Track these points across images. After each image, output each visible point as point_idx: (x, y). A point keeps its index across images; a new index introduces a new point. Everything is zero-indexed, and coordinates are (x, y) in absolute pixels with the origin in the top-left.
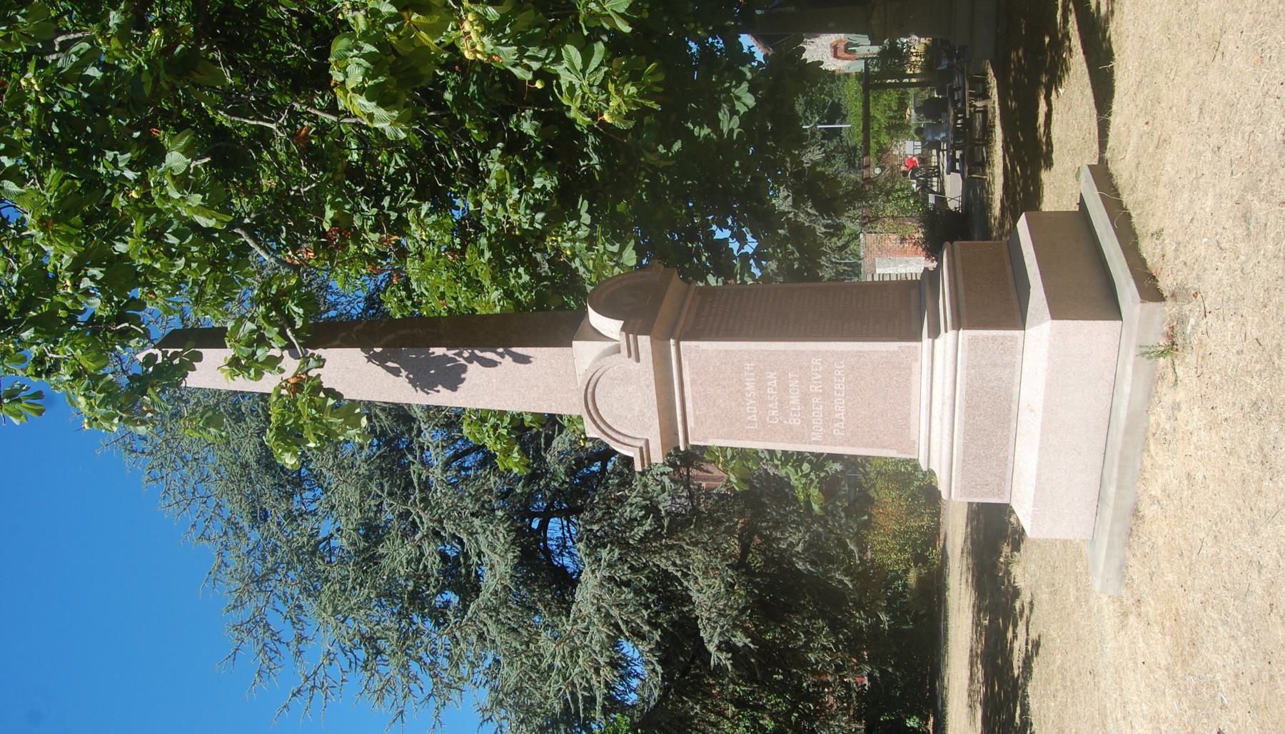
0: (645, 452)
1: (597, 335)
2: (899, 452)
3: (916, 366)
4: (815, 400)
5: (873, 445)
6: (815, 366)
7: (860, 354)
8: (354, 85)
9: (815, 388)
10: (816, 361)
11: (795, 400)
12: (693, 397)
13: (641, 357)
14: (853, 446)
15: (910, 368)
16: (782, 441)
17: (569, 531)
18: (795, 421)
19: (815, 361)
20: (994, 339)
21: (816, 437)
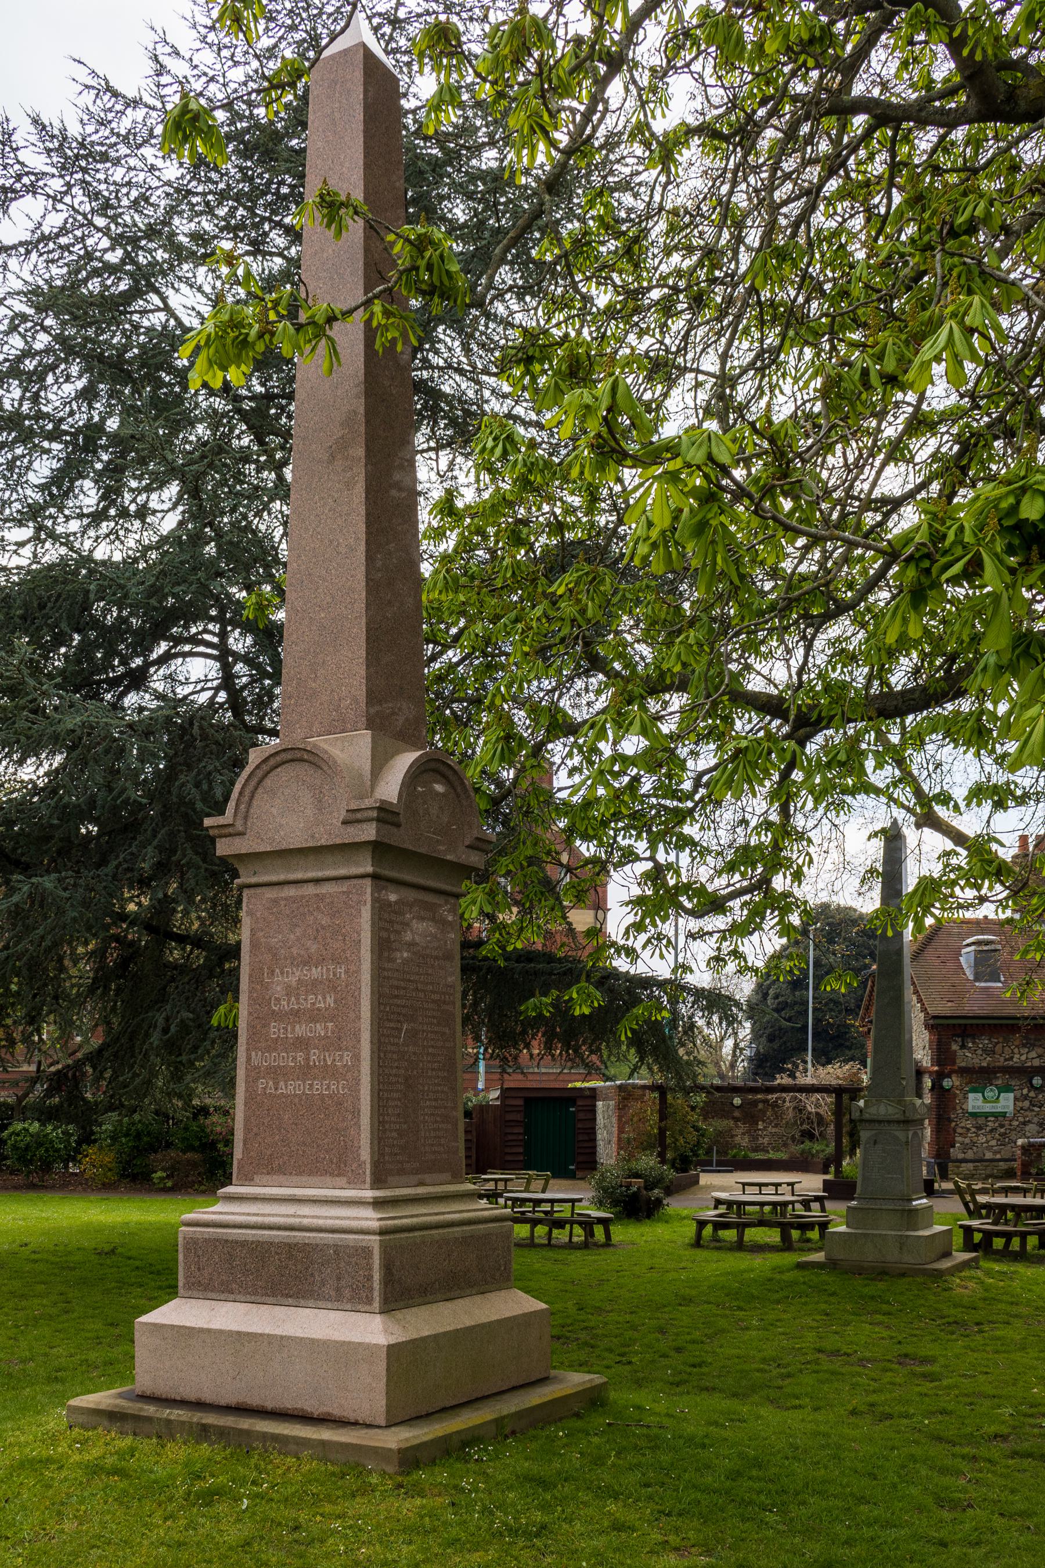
0: (229, 832)
1: (380, 763)
3: (342, 1181)
4: (300, 1056)
7: (356, 1113)
8: (965, 792)
11: (301, 1030)
17: (203, 690)
18: (275, 1030)
19: (347, 1058)
21: (256, 1058)
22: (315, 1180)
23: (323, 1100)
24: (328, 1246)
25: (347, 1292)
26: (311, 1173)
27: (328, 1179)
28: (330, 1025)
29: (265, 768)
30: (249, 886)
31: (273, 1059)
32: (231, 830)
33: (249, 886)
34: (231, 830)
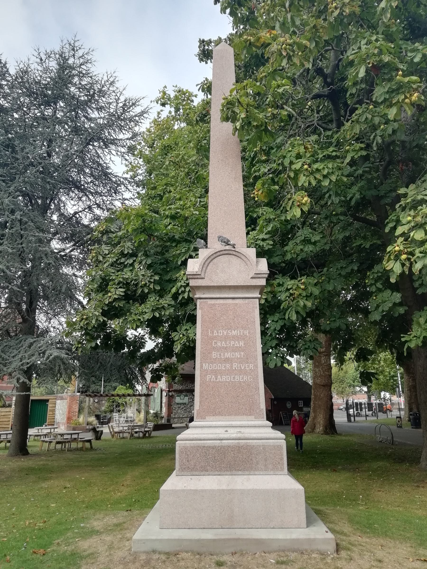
2: (198, 411)
4: (228, 366)
5: (201, 396)
6: (249, 366)
7: (258, 389)
9: (235, 365)
10: (251, 366)
11: (228, 355)
12: (226, 304)
13: (254, 280)
14: (200, 386)
15: (250, 415)
16: (202, 348)
18: (214, 355)
20: (282, 459)
21: (205, 366)
22: (239, 417)
23: (240, 384)
24: (260, 446)
25: (270, 466)
26: (236, 414)
27: (245, 417)
28: (242, 353)
29: (215, 255)
30: (200, 298)
31: (214, 367)
32: (198, 276)
33: (200, 298)
34: (198, 276)
